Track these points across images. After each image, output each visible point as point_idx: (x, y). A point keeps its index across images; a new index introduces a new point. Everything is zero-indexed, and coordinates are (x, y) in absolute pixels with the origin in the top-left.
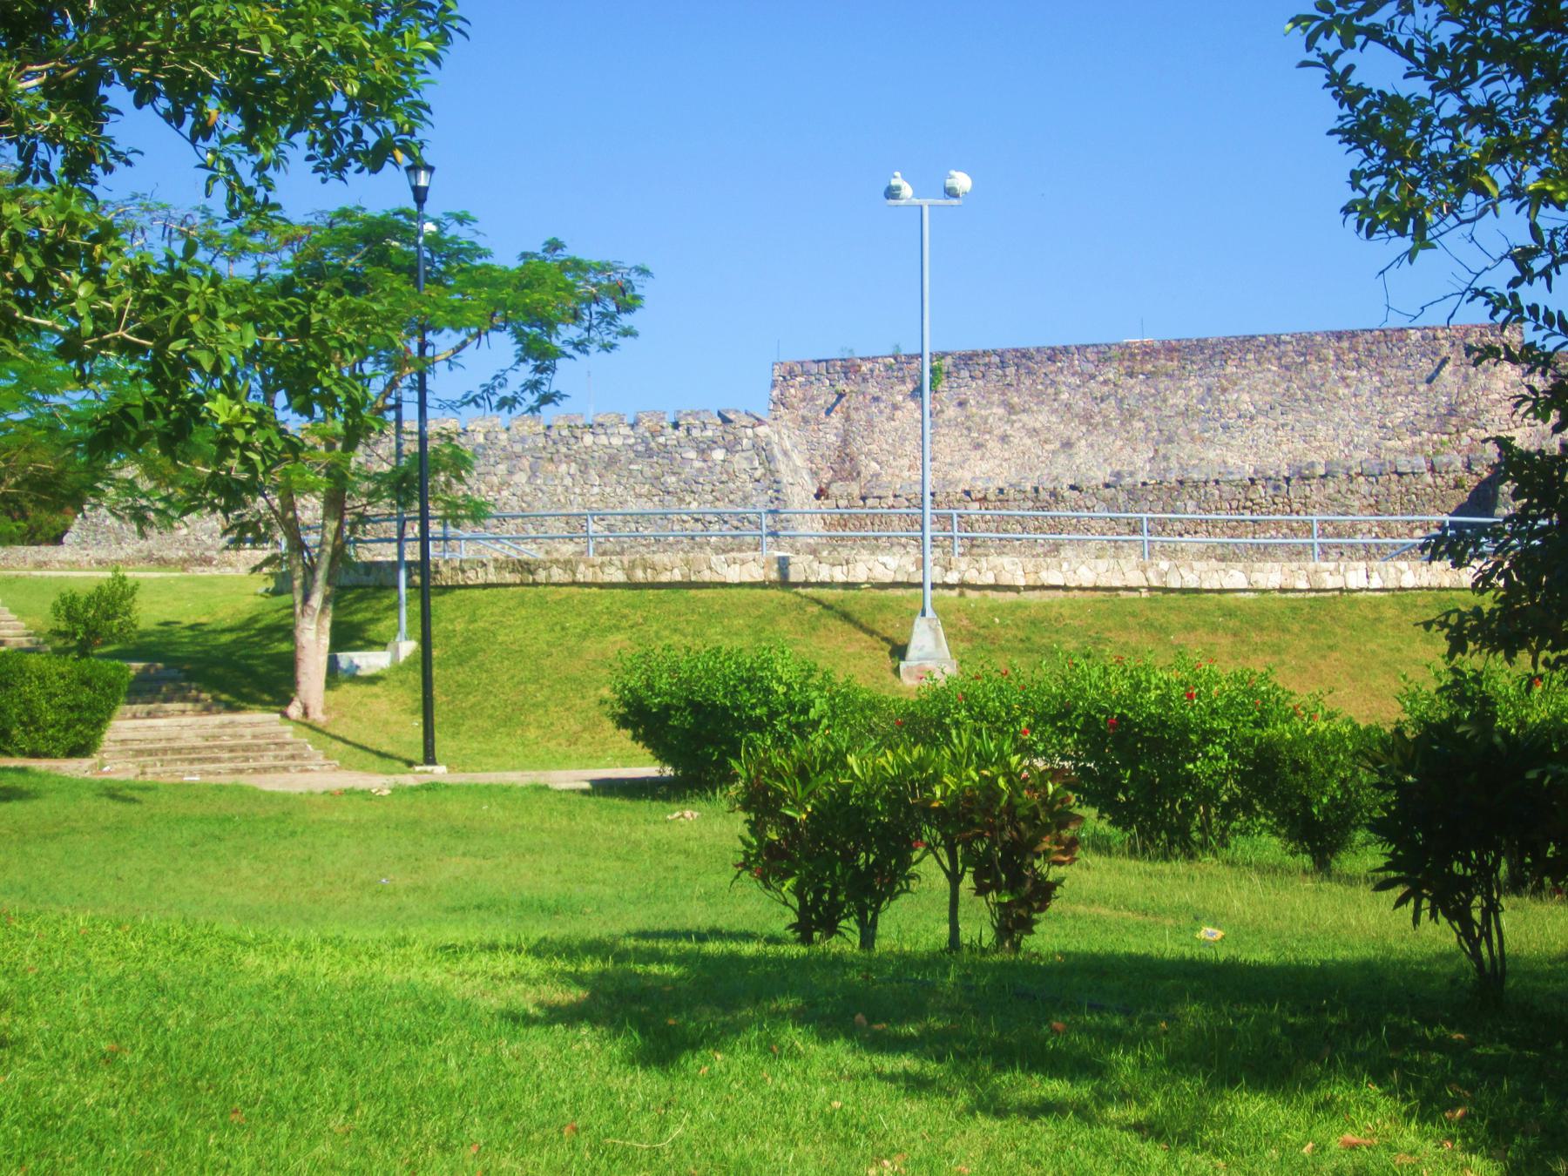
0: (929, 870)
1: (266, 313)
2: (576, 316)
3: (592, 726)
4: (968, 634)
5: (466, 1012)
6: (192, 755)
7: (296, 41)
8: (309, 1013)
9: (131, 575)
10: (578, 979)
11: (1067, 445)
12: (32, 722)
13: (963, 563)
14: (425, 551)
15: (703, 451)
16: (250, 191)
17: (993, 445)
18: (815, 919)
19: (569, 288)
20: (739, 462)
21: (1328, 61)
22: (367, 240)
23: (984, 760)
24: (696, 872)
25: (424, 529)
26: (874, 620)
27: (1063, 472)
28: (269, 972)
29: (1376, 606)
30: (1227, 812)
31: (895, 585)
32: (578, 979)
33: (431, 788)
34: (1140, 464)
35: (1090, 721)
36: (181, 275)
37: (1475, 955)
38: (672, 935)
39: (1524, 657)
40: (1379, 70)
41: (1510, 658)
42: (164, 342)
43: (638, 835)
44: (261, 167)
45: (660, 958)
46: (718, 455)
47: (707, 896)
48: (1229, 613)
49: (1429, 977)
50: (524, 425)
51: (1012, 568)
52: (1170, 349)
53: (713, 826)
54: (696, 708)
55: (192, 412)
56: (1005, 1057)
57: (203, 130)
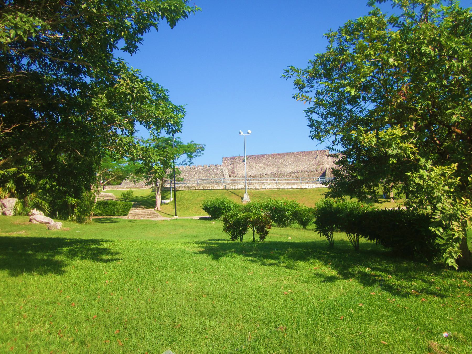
0: (250, 230)
1: (161, 154)
2: (195, 152)
3: (199, 210)
4: (252, 196)
5: (188, 253)
6: (142, 215)
7: (164, 116)
8: (165, 253)
9: (133, 189)
10: (203, 247)
11: (264, 168)
12: (118, 211)
13: (251, 186)
14: (175, 185)
15: (213, 170)
16: (156, 136)
17: (254, 168)
18: (234, 238)
19: (195, 148)
20: (218, 172)
21: (309, 116)
22: (165, 141)
23: (258, 214)
24: (216, 230)
25: (175, 182)
26: (239, 194)
27: (264, 172)
28: (159, 247)
29: (309, 191)
30: (291, 220)
31: (241, 189)
32: (203, 247)
33: (176, 219)
34: (275, 171)
35: (271, 208)
36: (148, 149)
37: (329, 240)
38: (214, 240)
39: (336, 199)
40: (315, 117)
41: (334, 199)
42: (146, 159)
43: (207, 225)
44: (158, 133)
45: (212, 244)
46: (215, 171)
47: (218, 234)
48: (289, 192)
49: (322, 244)
50: (187, 167)
51: (258, 186)
52: (279, 154)
53: (219, 224)
54: (214, 207)
55: (151, 168)
56: (265, 257)
57: (150, 128)
